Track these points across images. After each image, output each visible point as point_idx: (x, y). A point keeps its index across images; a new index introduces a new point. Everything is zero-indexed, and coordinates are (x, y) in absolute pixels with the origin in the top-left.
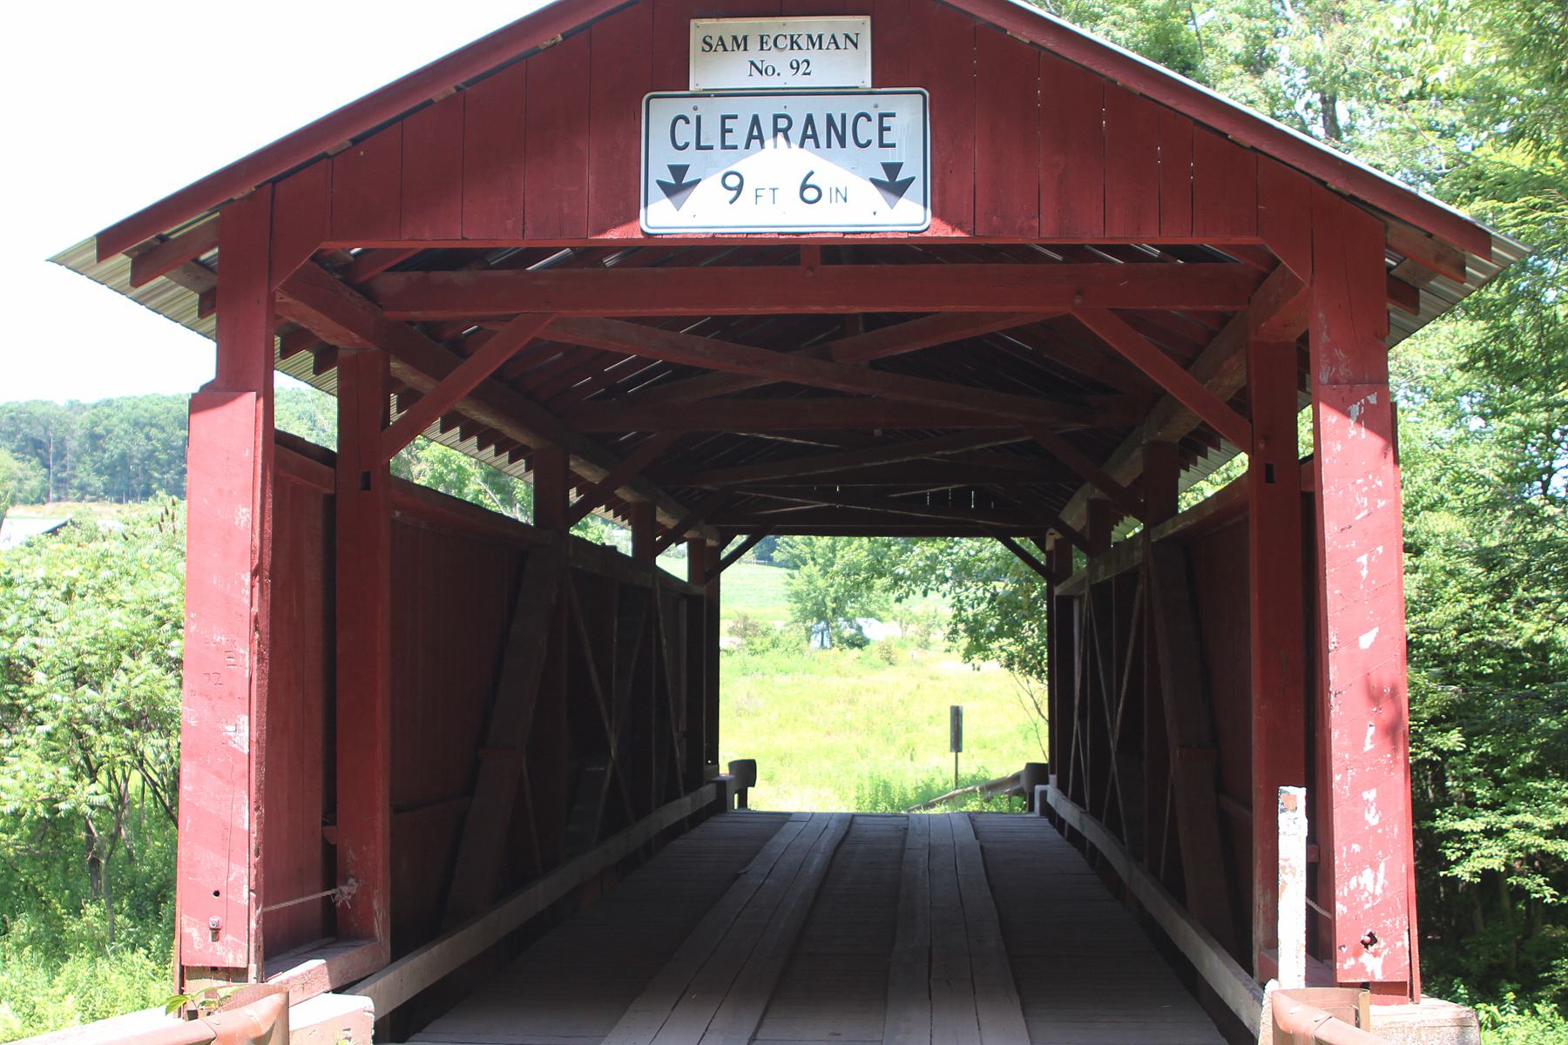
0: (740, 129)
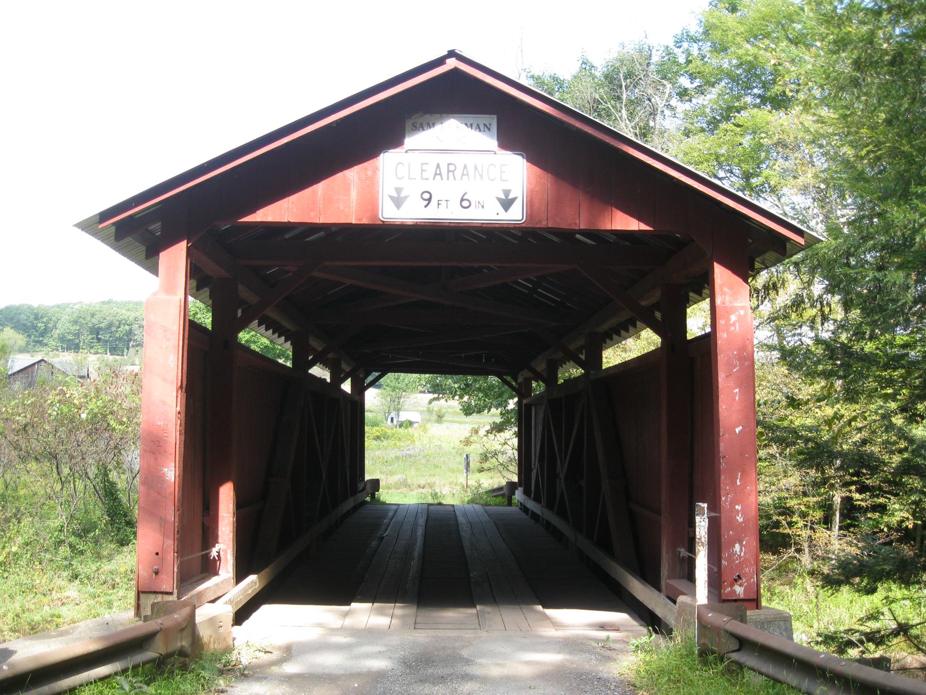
0: (431, 170)
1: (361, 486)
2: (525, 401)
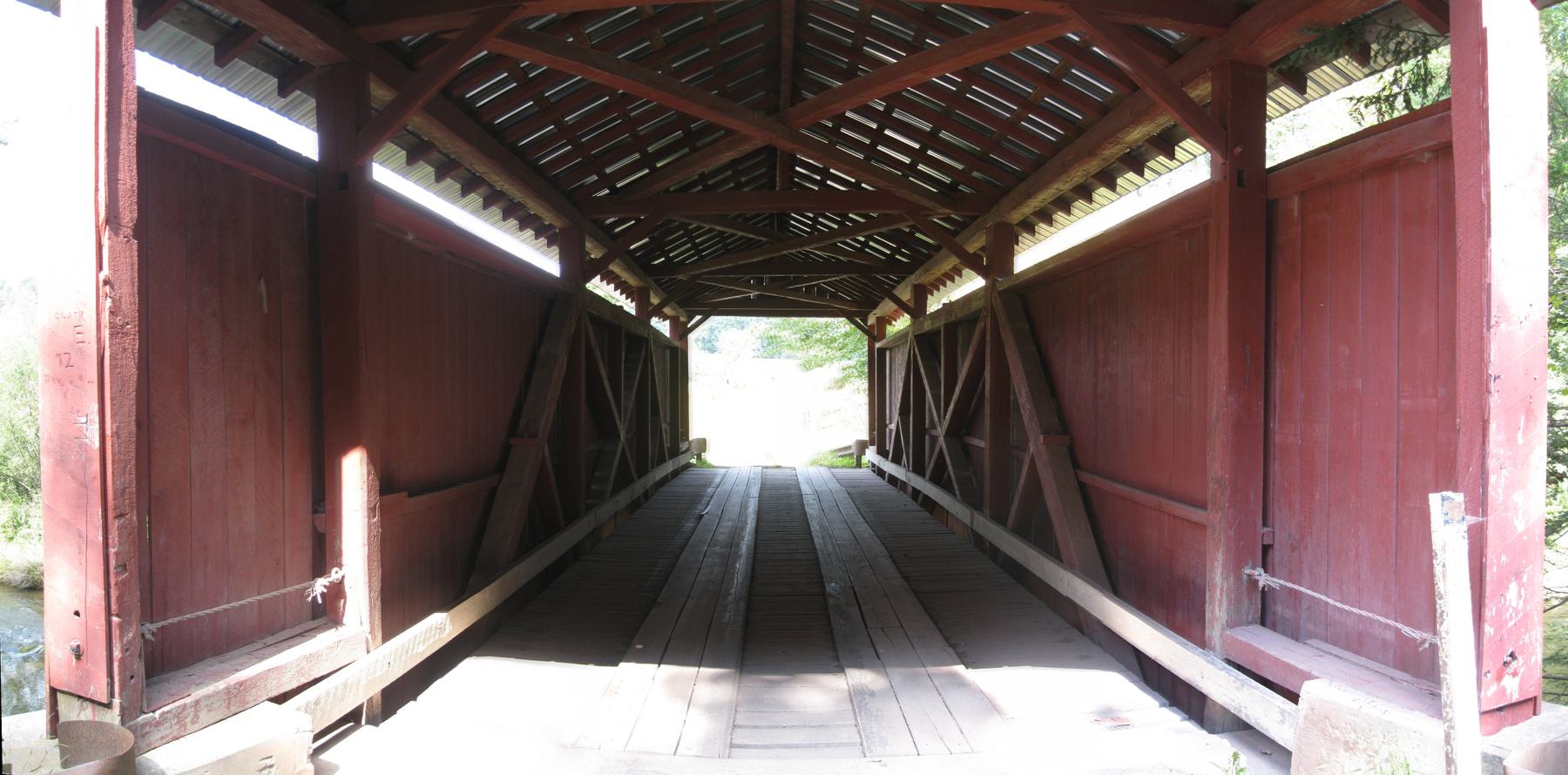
1: (684, 446)
2: (878, 345)
